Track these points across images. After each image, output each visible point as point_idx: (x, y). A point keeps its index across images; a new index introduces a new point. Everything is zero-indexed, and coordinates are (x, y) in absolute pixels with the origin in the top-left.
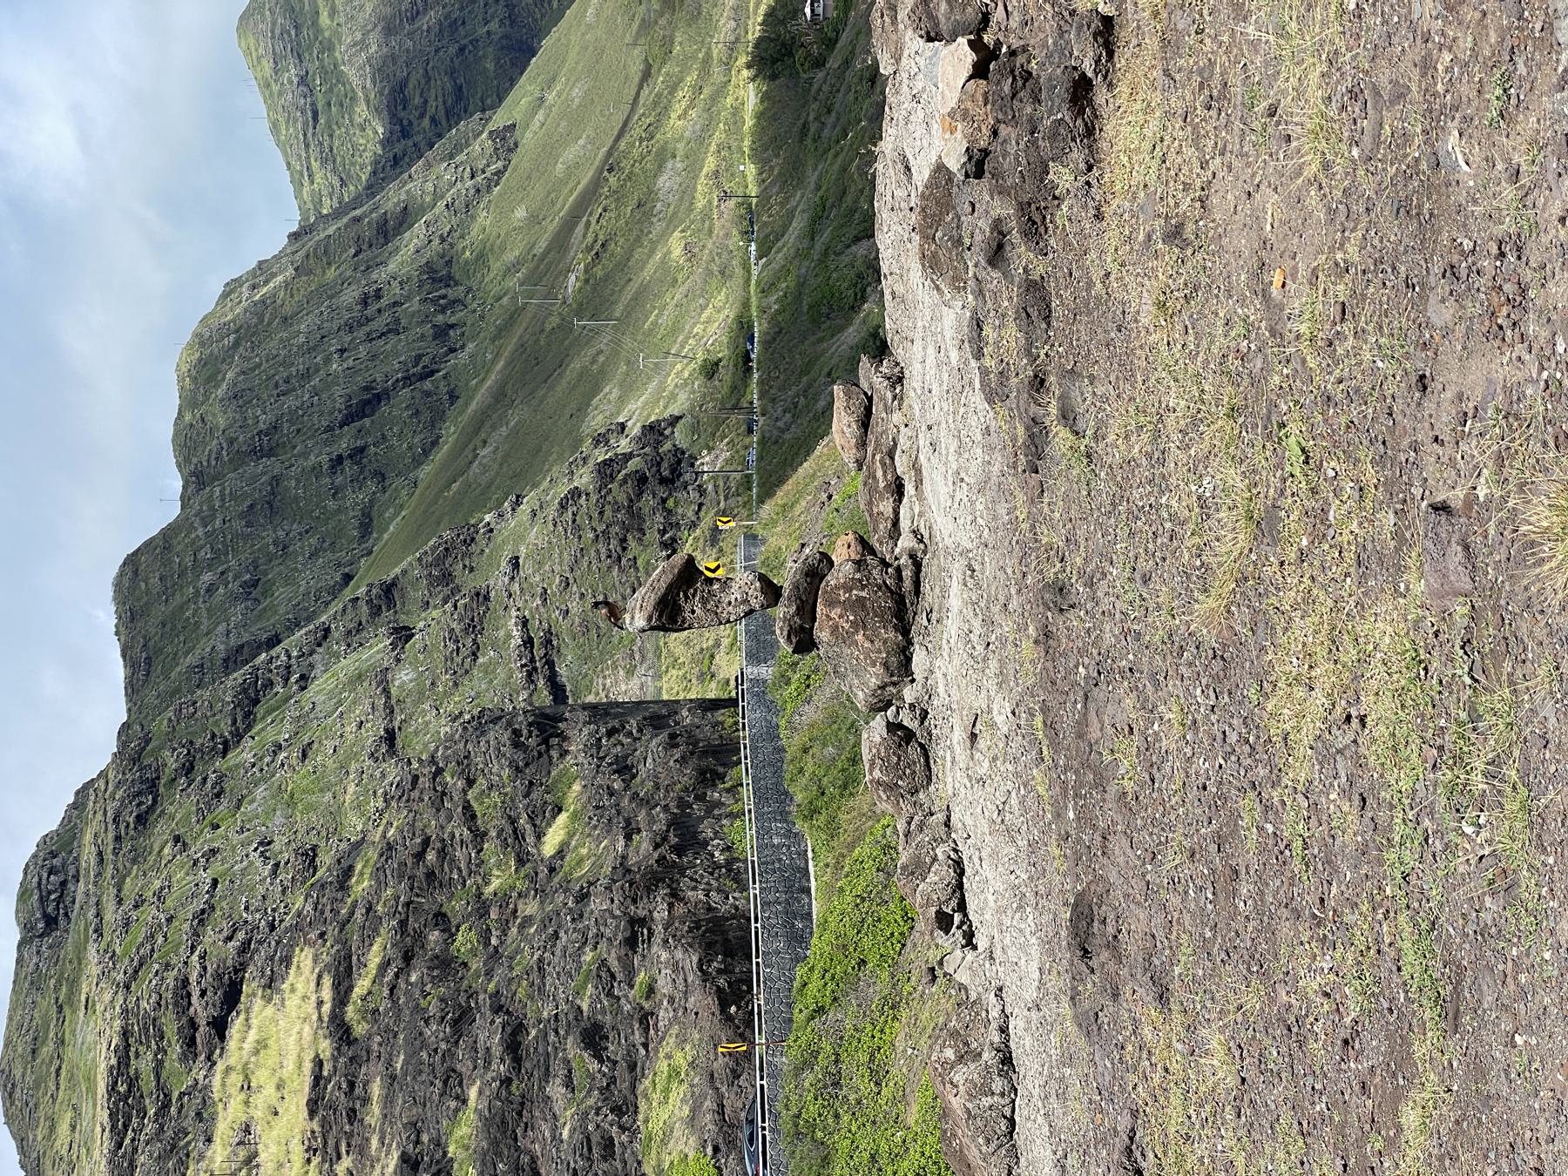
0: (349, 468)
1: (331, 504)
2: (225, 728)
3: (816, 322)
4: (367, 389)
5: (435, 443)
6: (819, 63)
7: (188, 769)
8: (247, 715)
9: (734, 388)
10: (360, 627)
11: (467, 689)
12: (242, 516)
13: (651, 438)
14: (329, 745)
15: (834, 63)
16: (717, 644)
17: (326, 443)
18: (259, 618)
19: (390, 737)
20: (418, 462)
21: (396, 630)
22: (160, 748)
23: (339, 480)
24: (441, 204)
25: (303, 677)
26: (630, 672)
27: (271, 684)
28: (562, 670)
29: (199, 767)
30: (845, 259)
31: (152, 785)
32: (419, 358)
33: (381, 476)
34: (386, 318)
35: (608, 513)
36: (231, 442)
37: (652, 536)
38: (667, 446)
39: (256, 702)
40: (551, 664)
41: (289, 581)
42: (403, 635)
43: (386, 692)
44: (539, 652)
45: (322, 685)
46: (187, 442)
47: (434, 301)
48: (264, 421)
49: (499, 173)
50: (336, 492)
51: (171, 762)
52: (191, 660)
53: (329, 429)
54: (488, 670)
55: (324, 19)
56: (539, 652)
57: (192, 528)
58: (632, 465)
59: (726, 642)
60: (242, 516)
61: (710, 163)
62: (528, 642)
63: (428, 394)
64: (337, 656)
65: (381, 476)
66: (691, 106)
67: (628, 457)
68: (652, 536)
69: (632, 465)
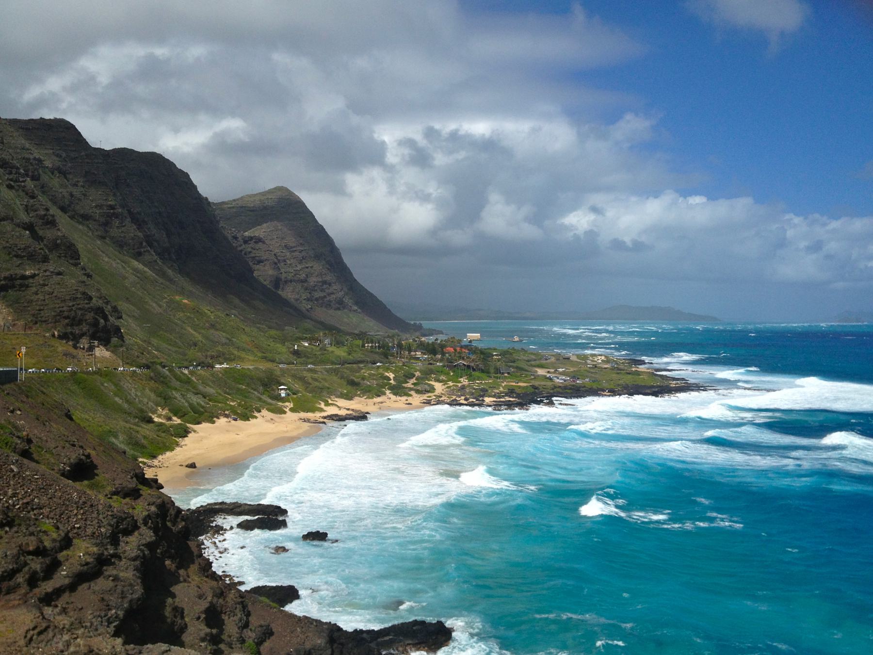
37: (69, 329)
68: (69, 329)
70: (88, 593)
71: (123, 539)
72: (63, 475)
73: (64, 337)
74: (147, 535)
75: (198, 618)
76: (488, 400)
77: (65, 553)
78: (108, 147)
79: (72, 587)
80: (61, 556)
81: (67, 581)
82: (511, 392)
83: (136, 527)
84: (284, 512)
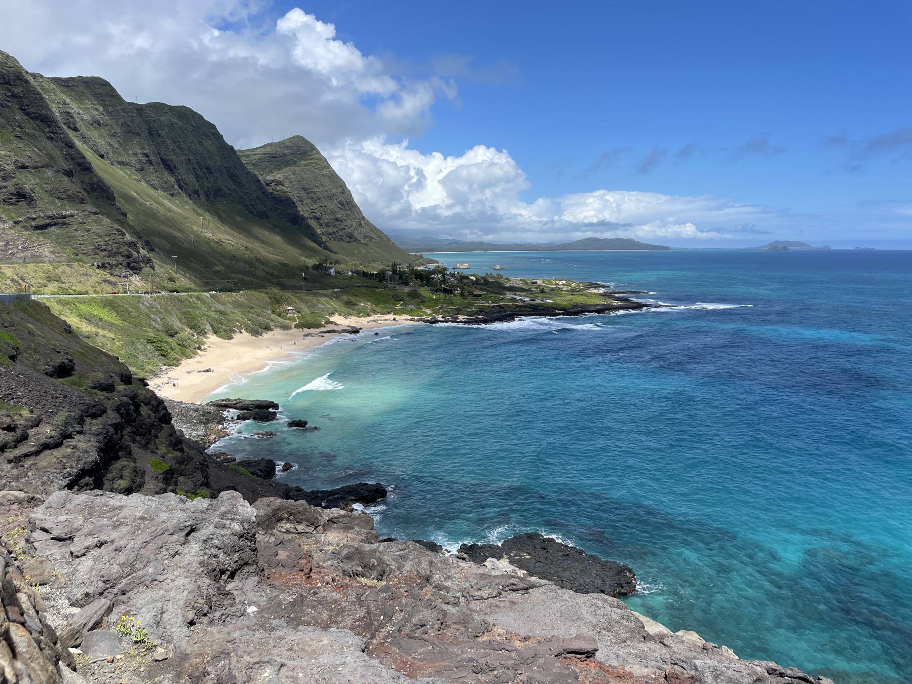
0: (145, 159)
1: (131, 152)
2: (31, 110)
3: (184, 313)
4: (175, 167)
5: (155, 188)
6: (273, 312)
7: (14, 96)
8: (37, 118)
9: (164, 287)
10: (73, 159)
11: (45, 196)
12: (125, 122)
13: (146, 260)
14: (21, 145)
15: (273, 316)
16: (63, 283)
17: (154, 153)
18: (85, 125)
19: (24, 167)
20: (147, 182)
21: (71, 171)
22: (23, 87)
23: (140, 156)
24: (242, 194)
25: (52, 138)
26: (52, 252)
27: (49, 127)
28: (53, 228)
29: (15, 100)
30: (205, 322)
31: (8, 83)
32: (187, 184)
33: (142, 169)
34: (202, 175)
35: (116, 245)
36: (154, 121)
37: (107, 260)
38: (142, 265)
39: (42, 121)
40: (55, 224)
41: (101, 136)
42: (69, 174)
43: (43, 167)
44: (60, 221)
45: (49, 144)
46: (158, 107)
47: (208, 190)
48: (163, 133)
49: (252, 213)
50: (135, 154)
51: (17, 90)
52: (68, 100)
53: (159, 154)
54: (52, 203)
55: (303, 162)
56: (60, 221)
57: (120, 105)
58: (135, 254)
59: (63, 285)
60: (125, 122)
61: (247, 278)
62: (64, 217)
63: (173, 187)
64: (61, 150)
65: (142, 169)
66: (267, 273)
67: (138, 252)
68: (107, 260)
69: (135, 254)
70: (48, 458)
71: (88, 420)
72: (47, 374)
73: (102, 267)
74: (112, 417)
75: (157, 478)
76: (461, 318)
77: (34, 430)
78: (142, 101)
79: (37, 453)
80: (32, 432)
81: (33, 449)
82: (481, 311)
83: (105, 412)
84: (276, 406)
